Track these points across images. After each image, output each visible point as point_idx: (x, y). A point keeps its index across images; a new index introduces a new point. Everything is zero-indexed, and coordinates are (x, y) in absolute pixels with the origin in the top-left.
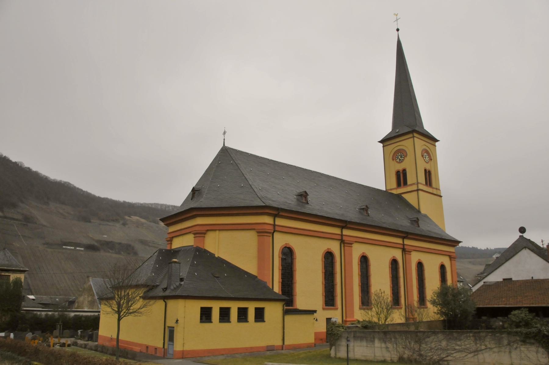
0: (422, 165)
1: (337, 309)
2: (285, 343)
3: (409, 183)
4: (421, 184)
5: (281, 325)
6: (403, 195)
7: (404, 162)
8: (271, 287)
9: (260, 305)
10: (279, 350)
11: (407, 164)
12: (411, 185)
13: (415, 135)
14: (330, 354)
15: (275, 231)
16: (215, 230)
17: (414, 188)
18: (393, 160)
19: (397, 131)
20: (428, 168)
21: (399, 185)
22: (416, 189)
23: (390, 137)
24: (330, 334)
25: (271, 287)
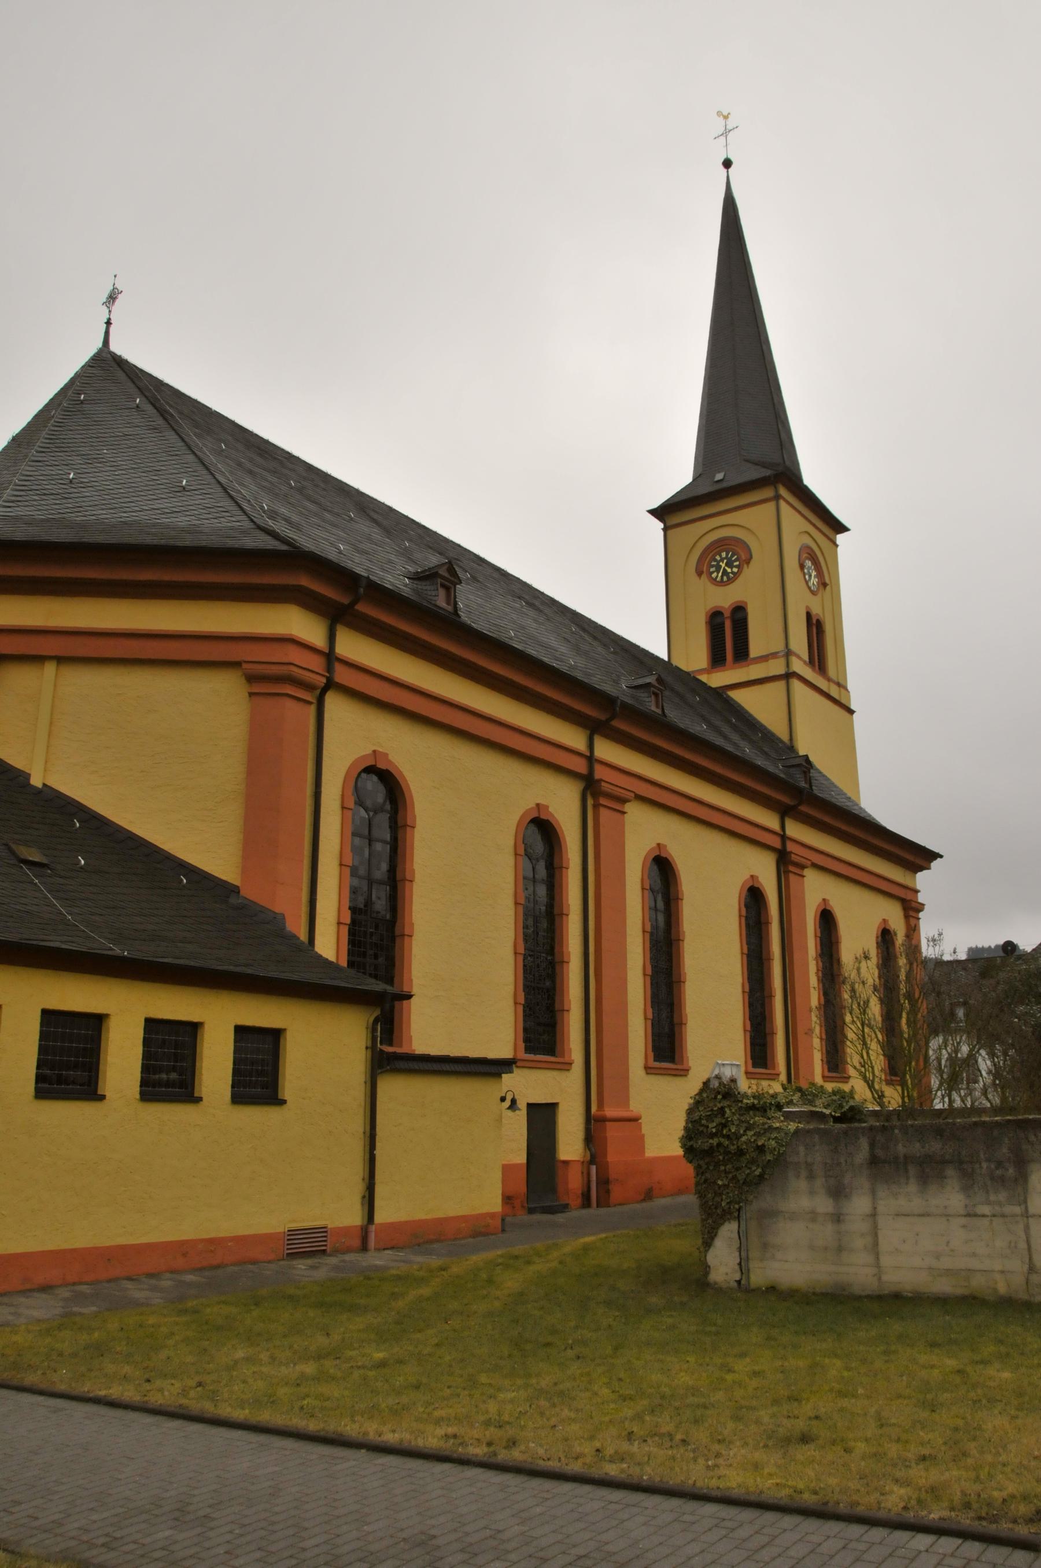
0: (799, 600)
1: (566, 1066)
2: (380, 1217)
3: (754, 652)
4: (799, 657)
5: (358, 1124)
6: (732, 694)
7: (737, 582)
8: (303, 936)
9: (261, 1012)
10: (349, 1250)
11: (751, 589)
12: (764, 658)
13: (783, 491)
14: (706, 1269)
15: (330, 684)
16: (39, 659)
17: (777, 667)
18: (699, 573)
19: (719, 476)
20: (816, 611)
21: (717, 659)
22: (781, 670)
23: (683, 497)
24: (710, 1152)
25: (303, 936)
